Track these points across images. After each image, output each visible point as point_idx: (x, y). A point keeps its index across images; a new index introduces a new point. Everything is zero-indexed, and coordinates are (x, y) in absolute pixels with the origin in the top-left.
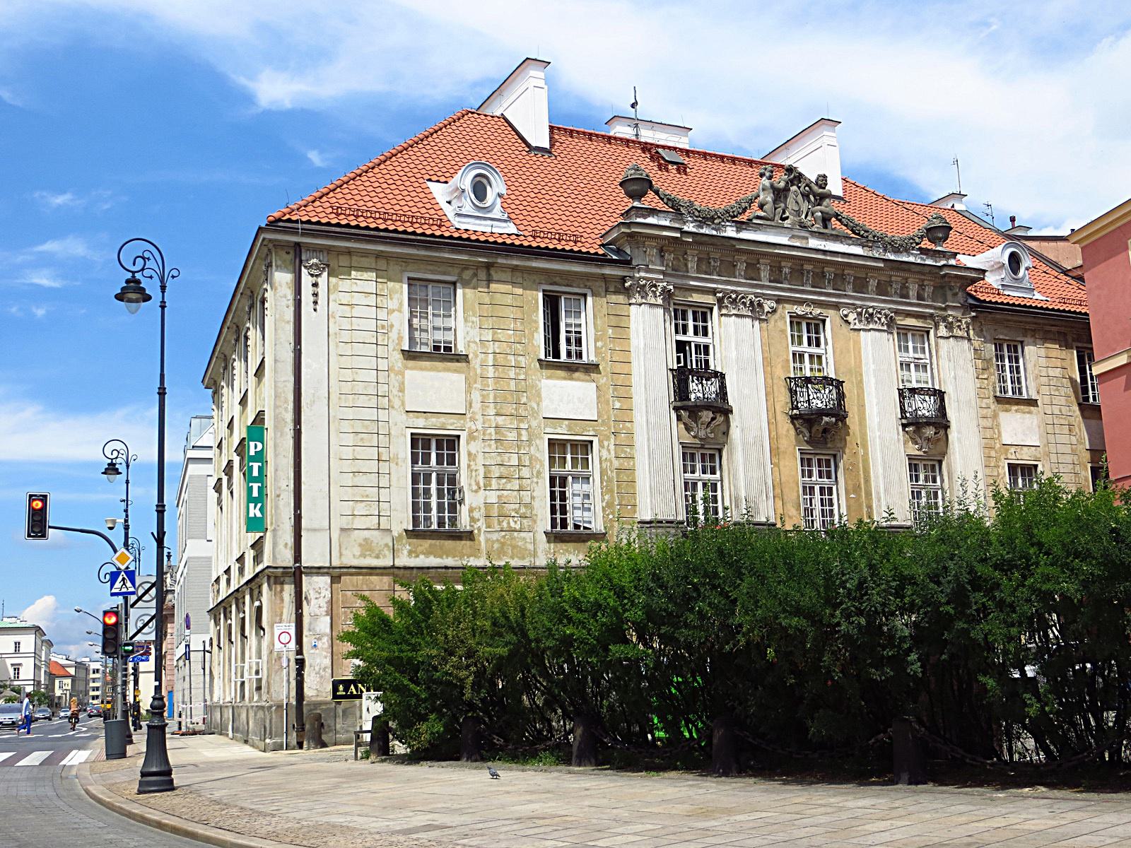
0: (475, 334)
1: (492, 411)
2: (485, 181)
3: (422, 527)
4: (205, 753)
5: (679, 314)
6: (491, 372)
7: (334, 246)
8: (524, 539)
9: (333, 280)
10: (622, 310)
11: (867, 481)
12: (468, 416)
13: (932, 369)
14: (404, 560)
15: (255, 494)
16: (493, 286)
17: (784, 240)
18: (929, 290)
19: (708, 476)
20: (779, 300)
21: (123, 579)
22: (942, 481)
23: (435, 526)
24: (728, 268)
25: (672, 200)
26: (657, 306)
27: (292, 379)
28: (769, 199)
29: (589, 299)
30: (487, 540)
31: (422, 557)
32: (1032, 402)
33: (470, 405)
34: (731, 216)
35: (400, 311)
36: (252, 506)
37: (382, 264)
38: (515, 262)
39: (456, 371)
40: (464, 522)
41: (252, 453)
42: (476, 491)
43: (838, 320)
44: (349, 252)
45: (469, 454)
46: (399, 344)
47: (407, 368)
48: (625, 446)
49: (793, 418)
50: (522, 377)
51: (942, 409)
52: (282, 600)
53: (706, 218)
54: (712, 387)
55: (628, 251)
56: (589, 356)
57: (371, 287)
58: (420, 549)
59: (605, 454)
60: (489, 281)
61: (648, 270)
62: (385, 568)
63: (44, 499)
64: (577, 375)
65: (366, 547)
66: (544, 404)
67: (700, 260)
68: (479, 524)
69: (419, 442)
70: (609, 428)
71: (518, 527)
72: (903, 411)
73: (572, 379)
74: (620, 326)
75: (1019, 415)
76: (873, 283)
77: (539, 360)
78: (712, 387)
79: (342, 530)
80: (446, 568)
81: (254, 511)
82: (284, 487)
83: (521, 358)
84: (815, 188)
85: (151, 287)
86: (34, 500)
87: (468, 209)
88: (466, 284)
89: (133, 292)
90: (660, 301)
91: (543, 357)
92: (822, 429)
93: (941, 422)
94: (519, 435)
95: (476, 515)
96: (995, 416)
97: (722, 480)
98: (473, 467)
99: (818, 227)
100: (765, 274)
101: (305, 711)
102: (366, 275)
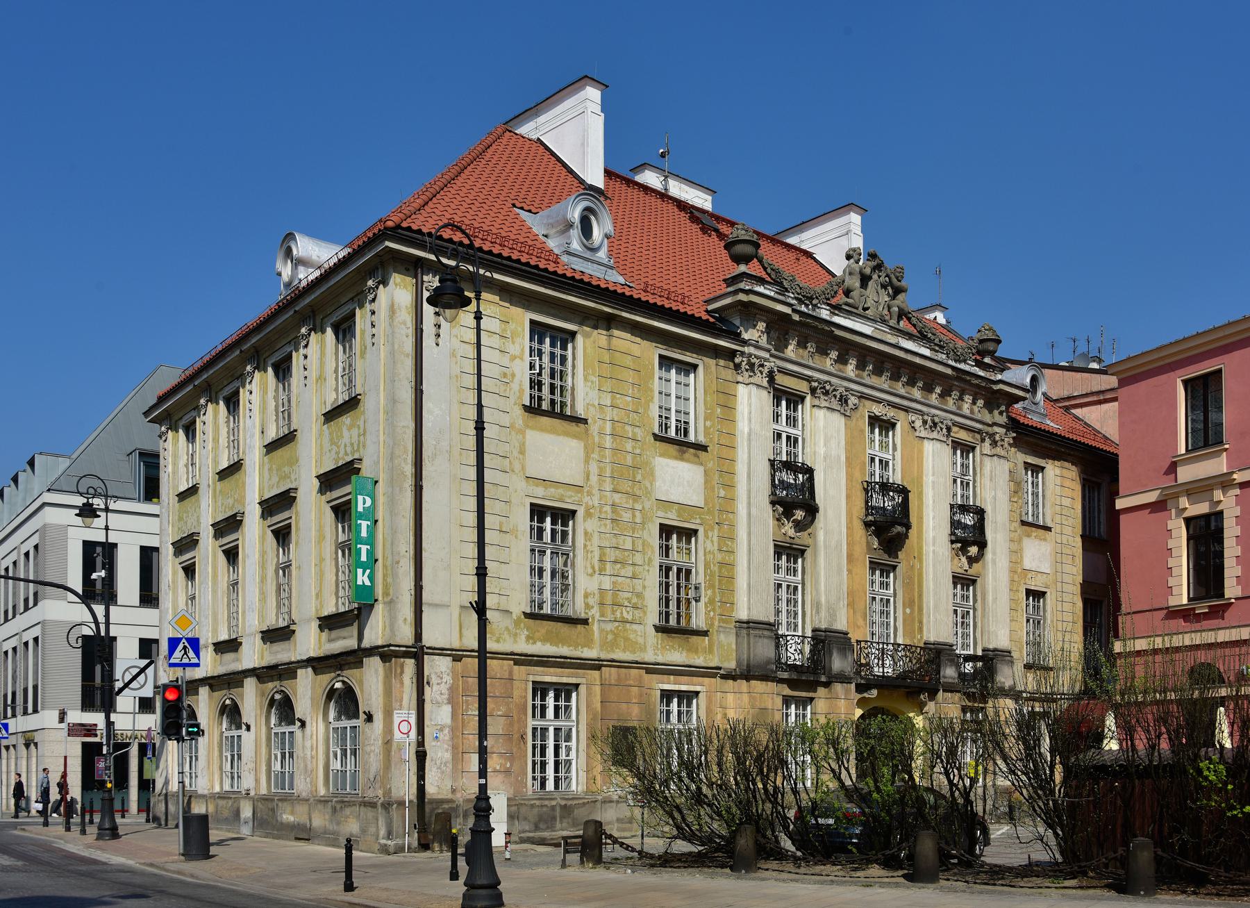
6: (608, 442)
11: (920, 596)
13: (974, 487)
15: (364, 558)
20: (862, 397)
21: (185, 648)
25: (777, 271)
31: (539, 644)
35: (522, 359)
40: (577, 608)
41: (360, 509)
42: (591, 575)
45: (586, 533)
46: (520, 397)
47: (527, 426)
48: (728, 538)
50: (638, 451)
55: (737, 322)
69: (538, 512)
71: (630, 618)
73: (682, 459)
83: (637, 430)
91: (657, 432)
94: (634, 516)
96: (1020, 541)
99: (893, 323)
101: (427, 809)
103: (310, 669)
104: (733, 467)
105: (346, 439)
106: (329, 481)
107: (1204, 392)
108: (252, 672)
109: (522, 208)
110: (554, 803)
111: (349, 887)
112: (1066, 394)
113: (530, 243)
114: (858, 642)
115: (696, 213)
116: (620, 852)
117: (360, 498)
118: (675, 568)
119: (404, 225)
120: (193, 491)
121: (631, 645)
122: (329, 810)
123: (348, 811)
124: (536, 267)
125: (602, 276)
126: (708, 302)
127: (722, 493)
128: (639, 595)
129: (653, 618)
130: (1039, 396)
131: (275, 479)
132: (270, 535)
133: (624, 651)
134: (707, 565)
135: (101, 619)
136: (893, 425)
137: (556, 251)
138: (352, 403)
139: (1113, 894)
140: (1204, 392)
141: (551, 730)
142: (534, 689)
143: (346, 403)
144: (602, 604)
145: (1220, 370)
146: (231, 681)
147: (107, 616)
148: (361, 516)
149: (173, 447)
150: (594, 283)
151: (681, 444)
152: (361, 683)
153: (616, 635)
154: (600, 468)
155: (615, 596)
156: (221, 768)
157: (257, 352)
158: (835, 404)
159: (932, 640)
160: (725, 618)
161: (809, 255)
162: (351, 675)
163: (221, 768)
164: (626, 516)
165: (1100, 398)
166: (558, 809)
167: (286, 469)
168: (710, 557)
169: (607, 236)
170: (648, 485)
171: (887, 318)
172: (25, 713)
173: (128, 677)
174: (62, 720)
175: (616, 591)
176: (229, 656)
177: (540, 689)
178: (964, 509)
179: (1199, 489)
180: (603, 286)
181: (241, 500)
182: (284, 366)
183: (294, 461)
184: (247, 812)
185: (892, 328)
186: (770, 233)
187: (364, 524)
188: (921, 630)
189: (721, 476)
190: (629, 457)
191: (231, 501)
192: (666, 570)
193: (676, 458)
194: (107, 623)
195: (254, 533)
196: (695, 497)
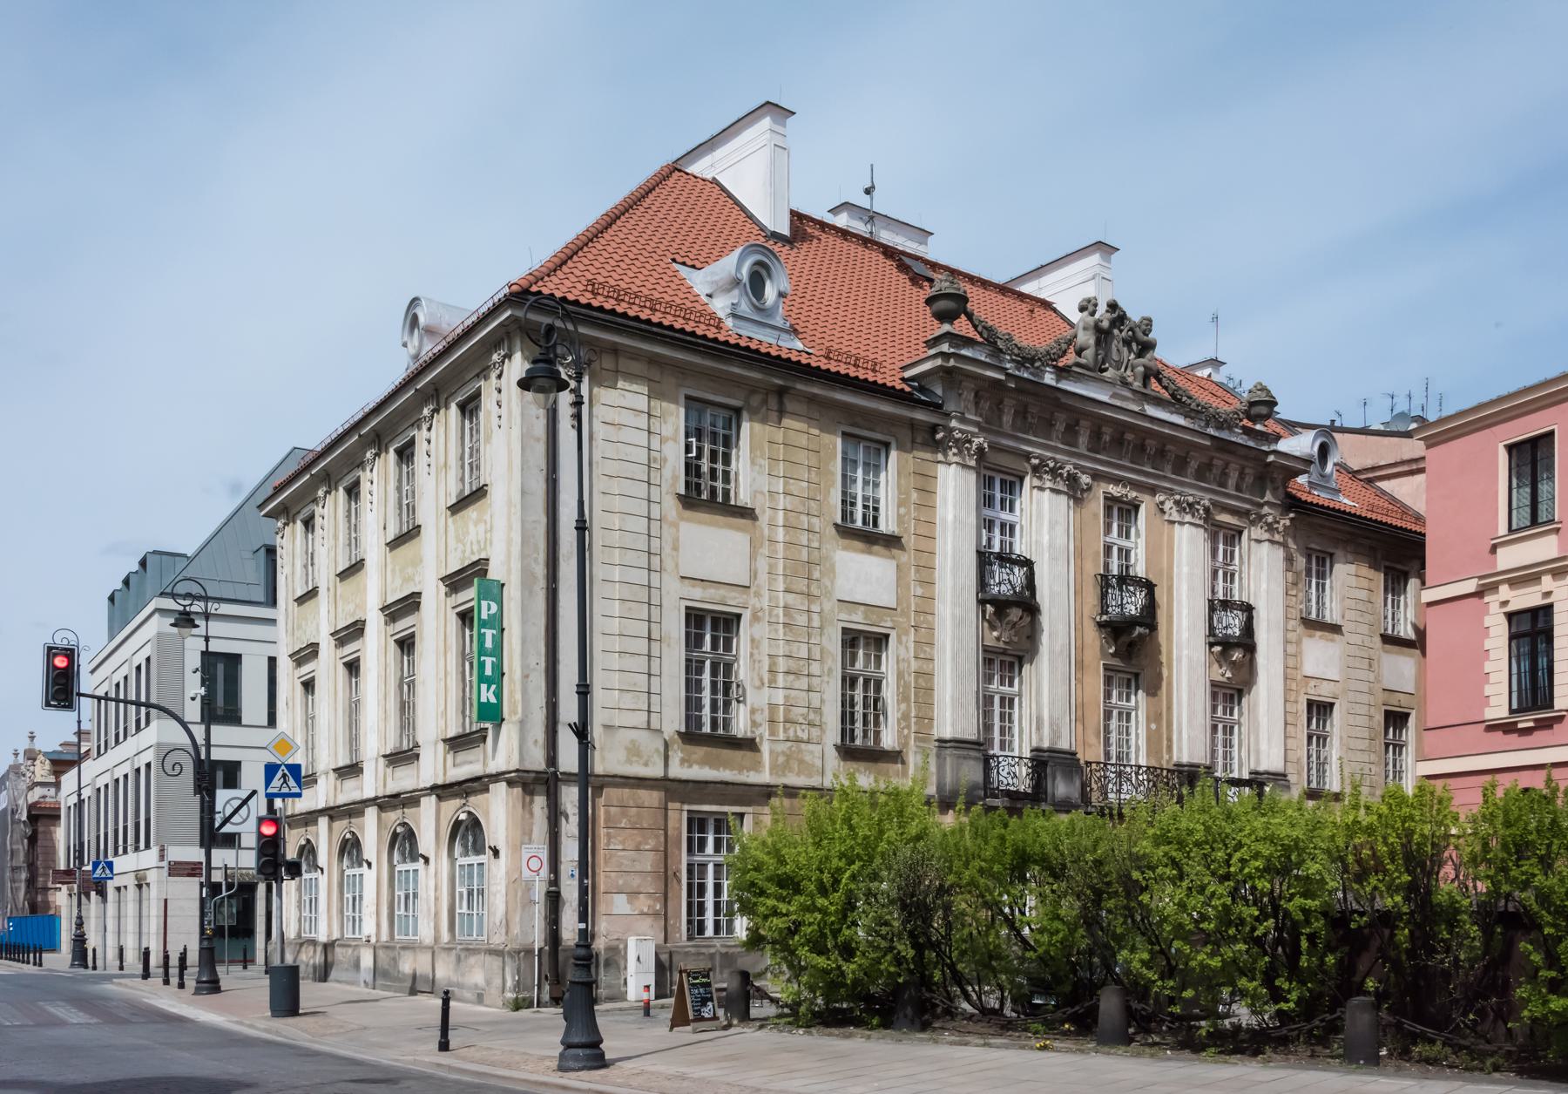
0: (764, 483)
1: (781, 587)
2: (764, 273)
3: (721, 731)
4: (52, 1010)
5: (986, 483)
6: (780, 534)
7: (597, 339)
8: (812, 752)
9: (596, 390)
10: (927, 468)
11: (1169, 708)
12: (753, 589)
13: (1241, 579)
14: (677, 771)
15: (488, 672)
16: (786, 422)
17: (1104, 398)
18: (1249, 480)
19: (1006, 689)
20: (1097, 476)
21: (284, 776)
22: (1241, 714)
23: (707, 729)
24: (1045, 427)
25: (989, 329)
26: (970, 467)
27: (544, 520)
28: (1092, 341)
29: (894, 454)
30: (771, 752)
31: (696, 767)
32: (1335, 629)
33: (754, 574)
34: (1051, 358)
35: (675, 440)
37: (655, 374)
38: (816, 390)
39: (738, 529)
40: (741, 725)
41: (484, 616)
42: (759, 688)
43: (1153, 509)
44: (615, 350)
45: (753, 640)
46: (673, 485)
47: (682, 519)
48: (926, 643)
49: (1101, 625)
50: (816, 545)
51: (1248, 629)
52: (531, 814)
53: (1026, 359)
54: (1018, 575)
55: (939, 392)
56: (887, 525)
57: (641, 402)
58: (694, 757)
59: (902, 651)
60: (782, 412)
61: (963, 420)
62: (656, 780)
63: (70, 653)
64: (876, 548)
65: (634, 751)
66: (840, 582)
67: (1016, 413)
68: (761, 730)
69: (695, 618)
70: (909, 618)
71: (805, 737)
72: (1211, 628)
73: (870, 553)
74: (926, 488)
75: (1322, 643)
76: (1194, 464)
77: (836, 525)
78: (1018, 575)
79: (606, 727)
80: (727, 783)
81: (488, 695)
82: (533, 665)
83: (815, 520)
84: (1140, 334)
86: (55, 655)
87: (745, 309)
88: (755, 414)
90: (973, 463)
91: (839, 521)
92: (1130, 644)
93: (1247, 642)
94: (810, 620)
96: (1299, 643)
97: (1020, 695)
98: (756, 657)
99: (1137, 385)
100: (1083, 440)
101: (561, 958)
102: (635, 387)
103: (434, 797)
104: (933, 560)
105: (472, 536)
106: (455, 582)
107: (1532, 458)
108: (373, 801)
109: (684, 264)
110: (712, 950)
111: (444, 1046)
112: (1369, 463)
113: (689, 304)
114: (1088, 763)
115: (907, 261)
116: (770, 1010)
117: (484, 604)
118: (861, 680)
119: (534, 289)
120: (312, 594)
121: (804, 767)
122: (453, 957)
123: (472, 960)
124: (693, 334)
125: (773, 341)
126: (904, 368)
127: (919, 592)
128: (818, 711)
129: (833, 735)
130: (1329, 467)
131: (398, 582)
132: (392, 646)
133: (798, 774)
134: (900, 675)
135: (200, 740)
136: (1137, 508)
137: (721, 314)
138: (479, 493)
139: (1187, 1053)
140: (1532, 458)
141: (711, 868)
142: (690, 821)
143: (472, 493)
144: (772, 721)
145: (1552, 433)
146: (354, 810)
147: (208, 738)
148: (483, 624)
149: (291, 542)
150: (763, 350)
151: (871, 538)
152: (487, 813)
153: (788, 757)
154: (771, 566)
155: (787, 712)
156: (342, 912)
157: (378, 436)
158: (1062, 487)
159: (1185, 760)
160: (922, 736)
161: (1047, 305)
162: (476, 803)
163: (342, 912)
164: (802, 619)
165: (1414, 467)
166: (718, 958)
167: (410, 570)
168: (903, 666)
169: (781, 295)
170: (828, 583)
171: (1130, 380)
172: (137, 849)
173: (229, 811)
174: (162, 858)
175: (789, 706)
176: (350, 784)
177: (697, 823)
178: (1227, 605)
179: (1526, 577)
180: (774, 353)
181: (362, 606)
182: (408, 452)
183: (417, 561)
184: (367, 960)
185: (1134, 391)
186: (999, 278)
187: (489, 634)
188: (1170, 748)
189: (917, 571)
190: (805, 551)
191: (351, 607)
192: (849, 681)
193: (863, 552)
194: (208, 745)
195: (375, 647)
196: (886, 596)
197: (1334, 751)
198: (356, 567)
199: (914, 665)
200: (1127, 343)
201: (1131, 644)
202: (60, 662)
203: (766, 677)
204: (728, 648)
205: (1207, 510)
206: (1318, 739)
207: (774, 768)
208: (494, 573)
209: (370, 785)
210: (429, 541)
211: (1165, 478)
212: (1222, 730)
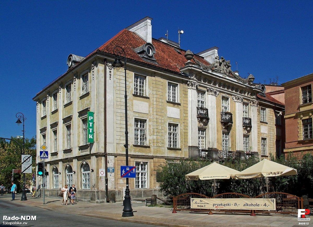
11: (235, 139)
15: (91, 132)
19: (202, 136)
22: (249, 141)
36: (90, 135)
39: (146, 102)
40: (147, 143)
47: (134, 99)
48: (186, 127)
51: (250, 123)
58: (137, 150)
71: (161, 146)
74: (186, 94)
75: (264, 126)
85: (22, 121)
89: (19, 121)
95: (151, 142)
96: (260, 126)
118: (172, 134)
120: (45, 117)
128: (163, 140)
129: (167, 145)
134: (181, 133)
136: (228, 99)
141: (140, 173)
152: (90, 163)
164: (160, 121)
166: (142, 192)
175: (157, 139)
179: (305, 113)
181: (58, 119)
187: (91, 123)
188: (235, 148)
192: (170, 134)
197: (267, 148)
198: (56, 111)
199: (184, 131)
200: (225, 66)
201: (228, 126)
202: (247, 122)
203: (152, 133)
204: (143, 127)
205: (242, 100)
206: (264, 145)
207: (154, 153)
208: (91, 110)
209: (61, 156)
210: (48, 118)
211: (234, 93)
212: (246, 143)
